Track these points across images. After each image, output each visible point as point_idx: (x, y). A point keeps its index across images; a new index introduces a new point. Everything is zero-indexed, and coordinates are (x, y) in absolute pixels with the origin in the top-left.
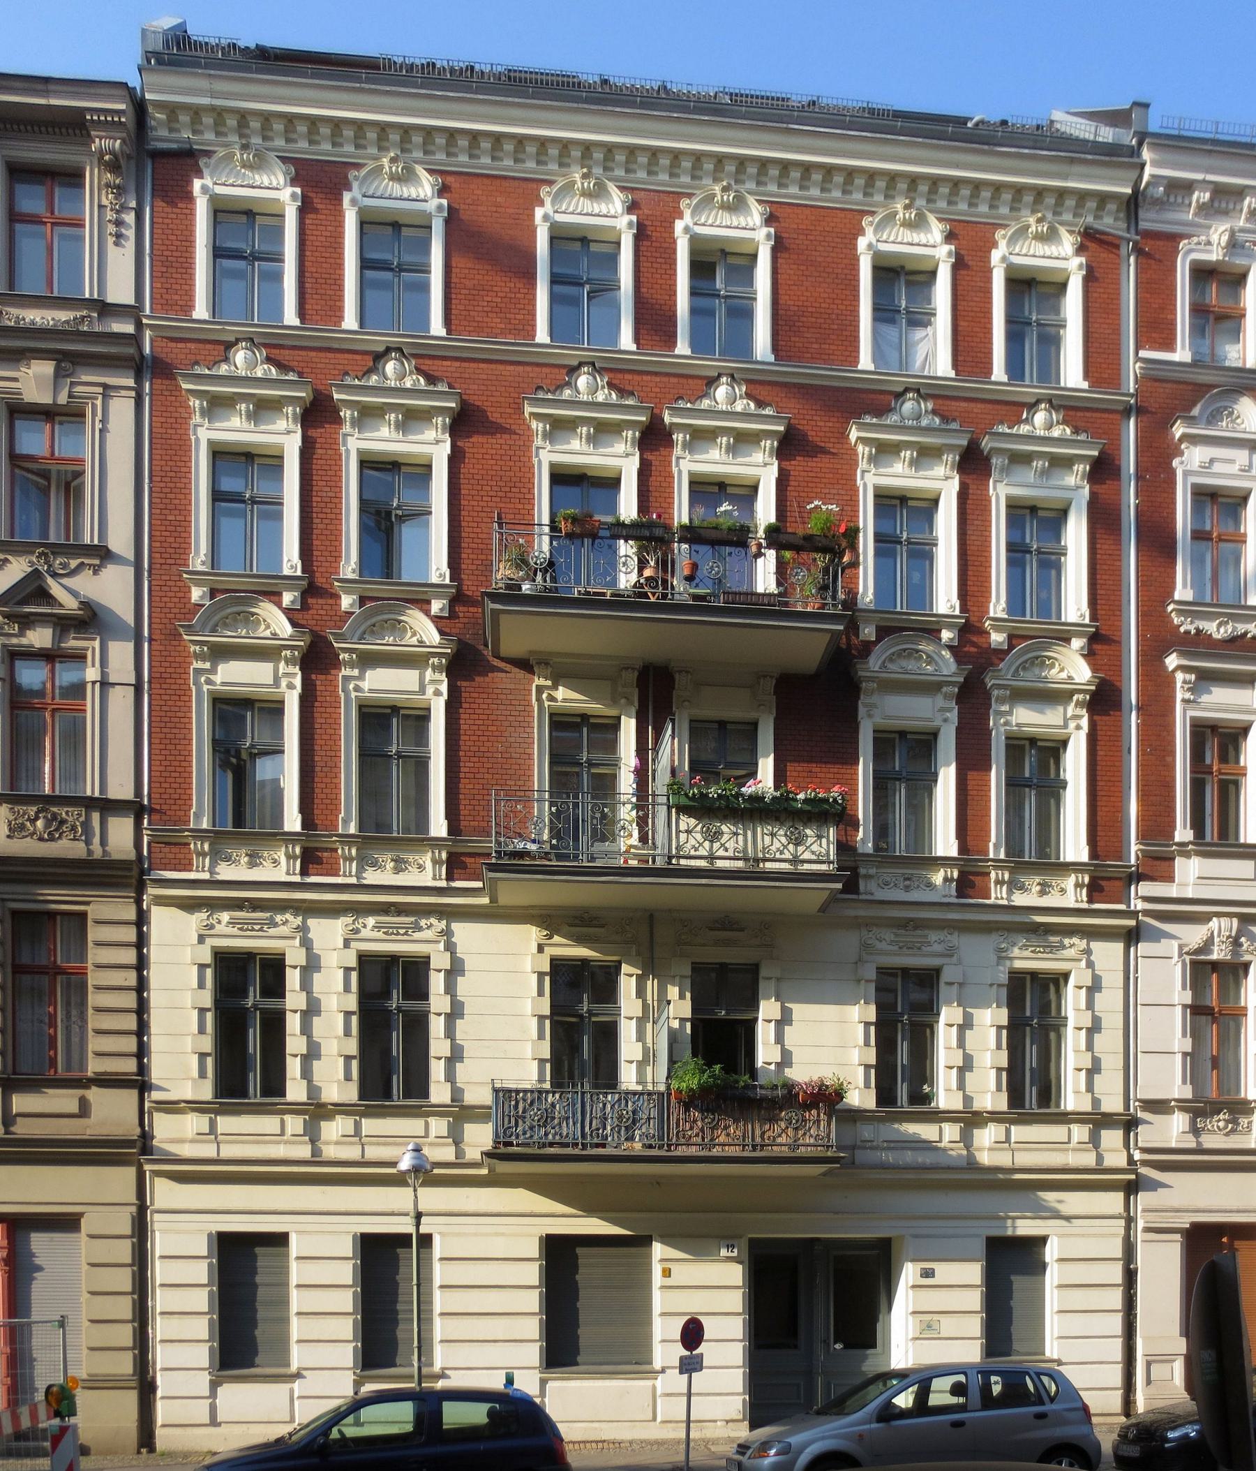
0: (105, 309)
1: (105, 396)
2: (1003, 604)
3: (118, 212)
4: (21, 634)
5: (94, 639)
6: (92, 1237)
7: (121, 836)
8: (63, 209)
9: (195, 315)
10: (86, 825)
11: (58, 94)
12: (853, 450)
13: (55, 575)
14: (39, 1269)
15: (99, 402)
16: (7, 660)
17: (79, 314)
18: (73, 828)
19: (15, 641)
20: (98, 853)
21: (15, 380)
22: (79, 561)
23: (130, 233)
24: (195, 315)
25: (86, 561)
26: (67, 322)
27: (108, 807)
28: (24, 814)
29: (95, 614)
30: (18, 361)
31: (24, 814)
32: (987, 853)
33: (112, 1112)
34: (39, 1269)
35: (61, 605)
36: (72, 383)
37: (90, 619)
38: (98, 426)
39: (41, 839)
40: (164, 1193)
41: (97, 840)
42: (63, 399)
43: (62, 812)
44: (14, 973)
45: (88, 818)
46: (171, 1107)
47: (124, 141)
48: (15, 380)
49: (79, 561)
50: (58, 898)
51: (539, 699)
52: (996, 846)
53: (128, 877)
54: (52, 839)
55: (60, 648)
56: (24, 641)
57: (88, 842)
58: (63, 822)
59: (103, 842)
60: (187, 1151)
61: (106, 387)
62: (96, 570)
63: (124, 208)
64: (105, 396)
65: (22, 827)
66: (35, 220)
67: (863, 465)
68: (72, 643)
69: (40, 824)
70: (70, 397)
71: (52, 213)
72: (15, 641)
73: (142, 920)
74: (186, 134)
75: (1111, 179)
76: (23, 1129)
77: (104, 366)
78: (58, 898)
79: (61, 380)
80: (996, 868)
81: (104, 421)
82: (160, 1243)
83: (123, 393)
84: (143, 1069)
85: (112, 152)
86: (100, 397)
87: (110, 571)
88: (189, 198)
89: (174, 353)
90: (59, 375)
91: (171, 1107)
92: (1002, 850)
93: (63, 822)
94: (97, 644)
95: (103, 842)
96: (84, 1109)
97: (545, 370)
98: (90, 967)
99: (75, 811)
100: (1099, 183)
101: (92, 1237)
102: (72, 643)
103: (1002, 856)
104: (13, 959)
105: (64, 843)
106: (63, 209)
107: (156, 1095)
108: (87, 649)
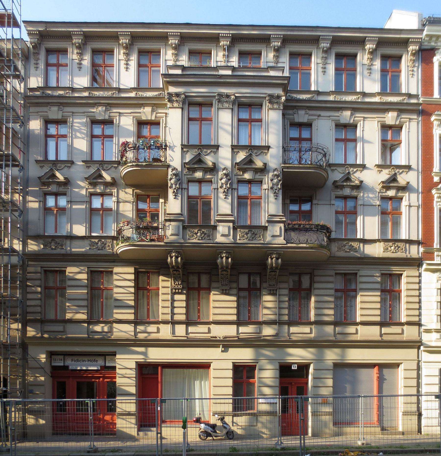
0: (410, 96)
1: (409, 122)
2: (438, 168)
3: (127, 61)
4: (386, 192)
5: (115, 189)
6: (214, 369)
7: (415, 252)
8: (154, 62)
9: (434, 97)
10: (405, 248)
11: (404, 34)
12: (432, 123)
13: (104, 170)
14: (386, 379)
15: (118, 118)
16: (43, 195)
17: (159, 93)
18: (402, 249)
19: (384, 194)
20: (409, 256)
21: (385, 118)
22: (402, 170)
23: (416, 74)
24: (434, 97)
25: (404, 170)
26: (156, 95)
27: (410, 242)
28: (388, 245)
29: (69, 181)
30: (339, 111)
31: (388, 245)
32: (433, 246)
33: (410, 333)
34: (386, 379)
35: (59, 179)
36: (156, 113)
37: (405, 188)
38: (164, 126)
39: (393, 252)
40: (425, 357)
41: (408, 252)
42: (153, 118)
43: (399, 244)
44: (91, 289)
45: (113, 242)
46: (428, 331)
47: (82, 40)
48: (385, 118)
49: (402, 170)
50: (396, 270)
51: (436, 205)
52: (437, 244)
53: (417, 263)
54: (396, 252)
55: (396, 196)
56: (386, 194)
57: (406, 253)
58: (399, 247)
59: (409, 253)
60: (433, 344)
61: (120, 113)
62: (361, 171)
63: (414, 66)
64: (364, 120)
65: (387, 249)
66: (145, 66)
67: (435, 127)
68: (400, 194)
69: (393, 248)
70: (400, 122)
71: (105, 63)
72: (384, 194)
73: (420, 276)
74: (433, 44)
75: (126, 27)
76: (294, 338)
77: (372, 112)
78: (396, 270)
79: (107, 112)
80: (436, 251)
81: (363, 127)
82: (424, 371)
83: (414, 120)
84: (420, 320)
85: (175, 44)
86: (408, 122)
87: (411, 173)
88: (432, 63)
89: (429, 109)
90: (153, 111)
91: (428, 331)
92: (438, 245)
93: (399, 247)
94: (116, 190)
95: (409, 253)
96: (209, 331)
97: (438, 106)
98: (160, 287)
99: (109, 240)
100: (192, 30)
101: (214, 369)
102: (400, 194)
103: (438, 247)
104: (91, 285)
105: (399, 253)
106: (108, 62)
107: (423, 328)
108: (404, 196)
